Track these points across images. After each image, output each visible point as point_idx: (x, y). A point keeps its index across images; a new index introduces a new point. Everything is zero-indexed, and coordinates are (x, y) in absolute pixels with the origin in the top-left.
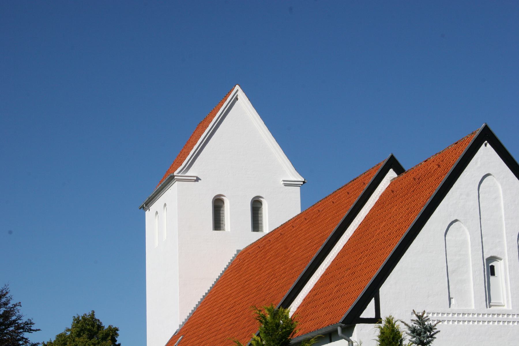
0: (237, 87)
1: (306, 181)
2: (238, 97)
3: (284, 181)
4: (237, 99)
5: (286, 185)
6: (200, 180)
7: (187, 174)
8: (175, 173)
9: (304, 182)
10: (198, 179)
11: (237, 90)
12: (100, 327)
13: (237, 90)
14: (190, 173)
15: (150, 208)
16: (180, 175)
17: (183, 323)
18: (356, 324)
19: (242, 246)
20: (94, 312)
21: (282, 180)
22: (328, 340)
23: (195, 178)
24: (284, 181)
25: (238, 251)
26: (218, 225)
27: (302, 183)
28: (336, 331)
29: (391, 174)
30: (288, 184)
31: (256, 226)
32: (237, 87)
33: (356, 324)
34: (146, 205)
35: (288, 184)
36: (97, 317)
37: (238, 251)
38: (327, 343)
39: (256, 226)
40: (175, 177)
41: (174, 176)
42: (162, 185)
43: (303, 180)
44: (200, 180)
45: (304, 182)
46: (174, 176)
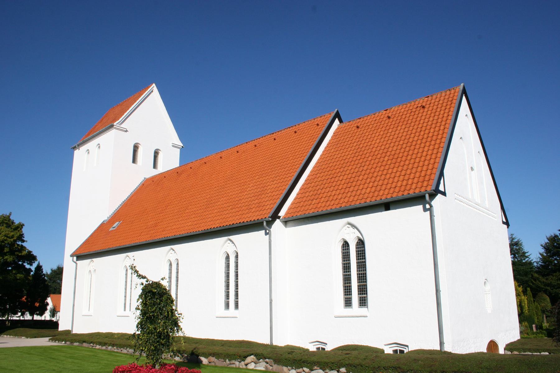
0: (154, 85)
1: (184, 147)
2: (153, 90)
3: (173, 144)
4: (152, 91)
5: (173, 146)
6: (128, 131)
7: (121, 126)
8: (115, 124)
9: (183, 147)
10: (126, 131)
11: (154, 87)
12: (13, 223)
13: (154, 87)
14: (122, 126)
15: (80, 148)
16: (117, 125)
17: (110, 216)
18: (439, 194)
19: (148, 176)
20: (11, 213)
21: (172, 143)
22: (384, 208)
23: (126, 130)
24: (173, 144)
25: (145, 178)
26: (134, 161)
27: (182, 147)
28: (263, 223)
29: (337, 122)
30: (174, 146)
31: (155, 166)
32: (154, 85)
33: (439, 194)
34: (78, 146)
35: (174, 146)
36: (12, 218)
37: (145, 178)
38: (381, 211)
39: (155, 166)
40: (114, 126)
41: (114, 125)
42: (100, 132)
43: (182, 146)
44: (128, 131)
45: (183, 147)
46: (114, 125)
